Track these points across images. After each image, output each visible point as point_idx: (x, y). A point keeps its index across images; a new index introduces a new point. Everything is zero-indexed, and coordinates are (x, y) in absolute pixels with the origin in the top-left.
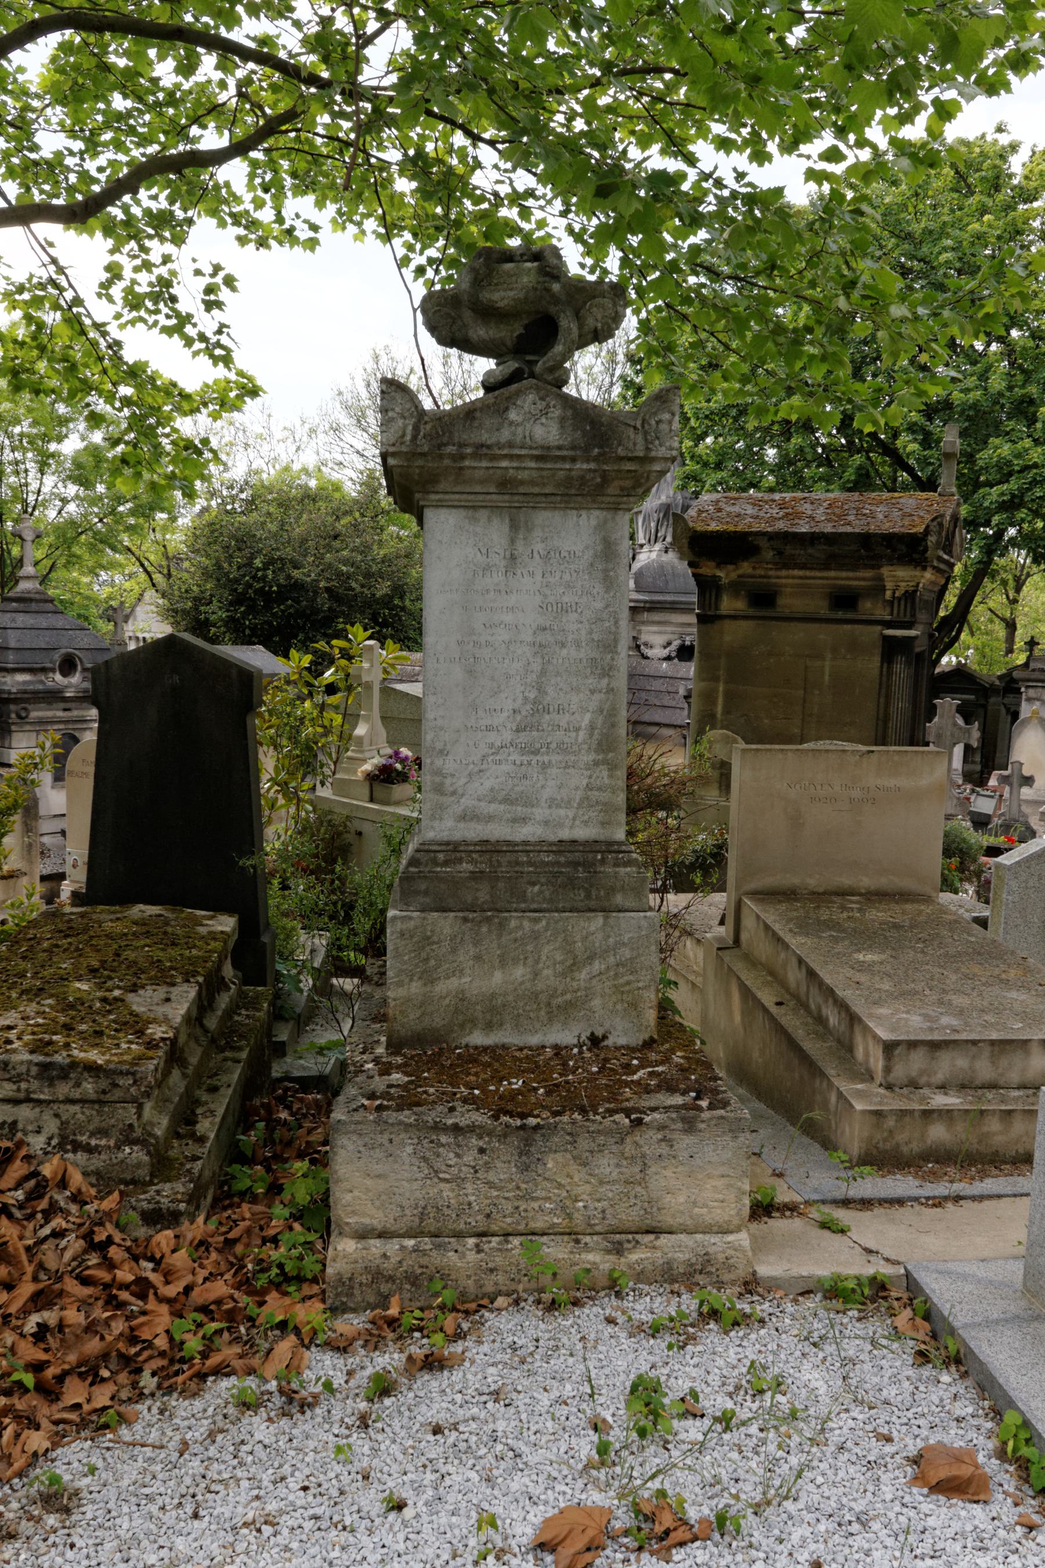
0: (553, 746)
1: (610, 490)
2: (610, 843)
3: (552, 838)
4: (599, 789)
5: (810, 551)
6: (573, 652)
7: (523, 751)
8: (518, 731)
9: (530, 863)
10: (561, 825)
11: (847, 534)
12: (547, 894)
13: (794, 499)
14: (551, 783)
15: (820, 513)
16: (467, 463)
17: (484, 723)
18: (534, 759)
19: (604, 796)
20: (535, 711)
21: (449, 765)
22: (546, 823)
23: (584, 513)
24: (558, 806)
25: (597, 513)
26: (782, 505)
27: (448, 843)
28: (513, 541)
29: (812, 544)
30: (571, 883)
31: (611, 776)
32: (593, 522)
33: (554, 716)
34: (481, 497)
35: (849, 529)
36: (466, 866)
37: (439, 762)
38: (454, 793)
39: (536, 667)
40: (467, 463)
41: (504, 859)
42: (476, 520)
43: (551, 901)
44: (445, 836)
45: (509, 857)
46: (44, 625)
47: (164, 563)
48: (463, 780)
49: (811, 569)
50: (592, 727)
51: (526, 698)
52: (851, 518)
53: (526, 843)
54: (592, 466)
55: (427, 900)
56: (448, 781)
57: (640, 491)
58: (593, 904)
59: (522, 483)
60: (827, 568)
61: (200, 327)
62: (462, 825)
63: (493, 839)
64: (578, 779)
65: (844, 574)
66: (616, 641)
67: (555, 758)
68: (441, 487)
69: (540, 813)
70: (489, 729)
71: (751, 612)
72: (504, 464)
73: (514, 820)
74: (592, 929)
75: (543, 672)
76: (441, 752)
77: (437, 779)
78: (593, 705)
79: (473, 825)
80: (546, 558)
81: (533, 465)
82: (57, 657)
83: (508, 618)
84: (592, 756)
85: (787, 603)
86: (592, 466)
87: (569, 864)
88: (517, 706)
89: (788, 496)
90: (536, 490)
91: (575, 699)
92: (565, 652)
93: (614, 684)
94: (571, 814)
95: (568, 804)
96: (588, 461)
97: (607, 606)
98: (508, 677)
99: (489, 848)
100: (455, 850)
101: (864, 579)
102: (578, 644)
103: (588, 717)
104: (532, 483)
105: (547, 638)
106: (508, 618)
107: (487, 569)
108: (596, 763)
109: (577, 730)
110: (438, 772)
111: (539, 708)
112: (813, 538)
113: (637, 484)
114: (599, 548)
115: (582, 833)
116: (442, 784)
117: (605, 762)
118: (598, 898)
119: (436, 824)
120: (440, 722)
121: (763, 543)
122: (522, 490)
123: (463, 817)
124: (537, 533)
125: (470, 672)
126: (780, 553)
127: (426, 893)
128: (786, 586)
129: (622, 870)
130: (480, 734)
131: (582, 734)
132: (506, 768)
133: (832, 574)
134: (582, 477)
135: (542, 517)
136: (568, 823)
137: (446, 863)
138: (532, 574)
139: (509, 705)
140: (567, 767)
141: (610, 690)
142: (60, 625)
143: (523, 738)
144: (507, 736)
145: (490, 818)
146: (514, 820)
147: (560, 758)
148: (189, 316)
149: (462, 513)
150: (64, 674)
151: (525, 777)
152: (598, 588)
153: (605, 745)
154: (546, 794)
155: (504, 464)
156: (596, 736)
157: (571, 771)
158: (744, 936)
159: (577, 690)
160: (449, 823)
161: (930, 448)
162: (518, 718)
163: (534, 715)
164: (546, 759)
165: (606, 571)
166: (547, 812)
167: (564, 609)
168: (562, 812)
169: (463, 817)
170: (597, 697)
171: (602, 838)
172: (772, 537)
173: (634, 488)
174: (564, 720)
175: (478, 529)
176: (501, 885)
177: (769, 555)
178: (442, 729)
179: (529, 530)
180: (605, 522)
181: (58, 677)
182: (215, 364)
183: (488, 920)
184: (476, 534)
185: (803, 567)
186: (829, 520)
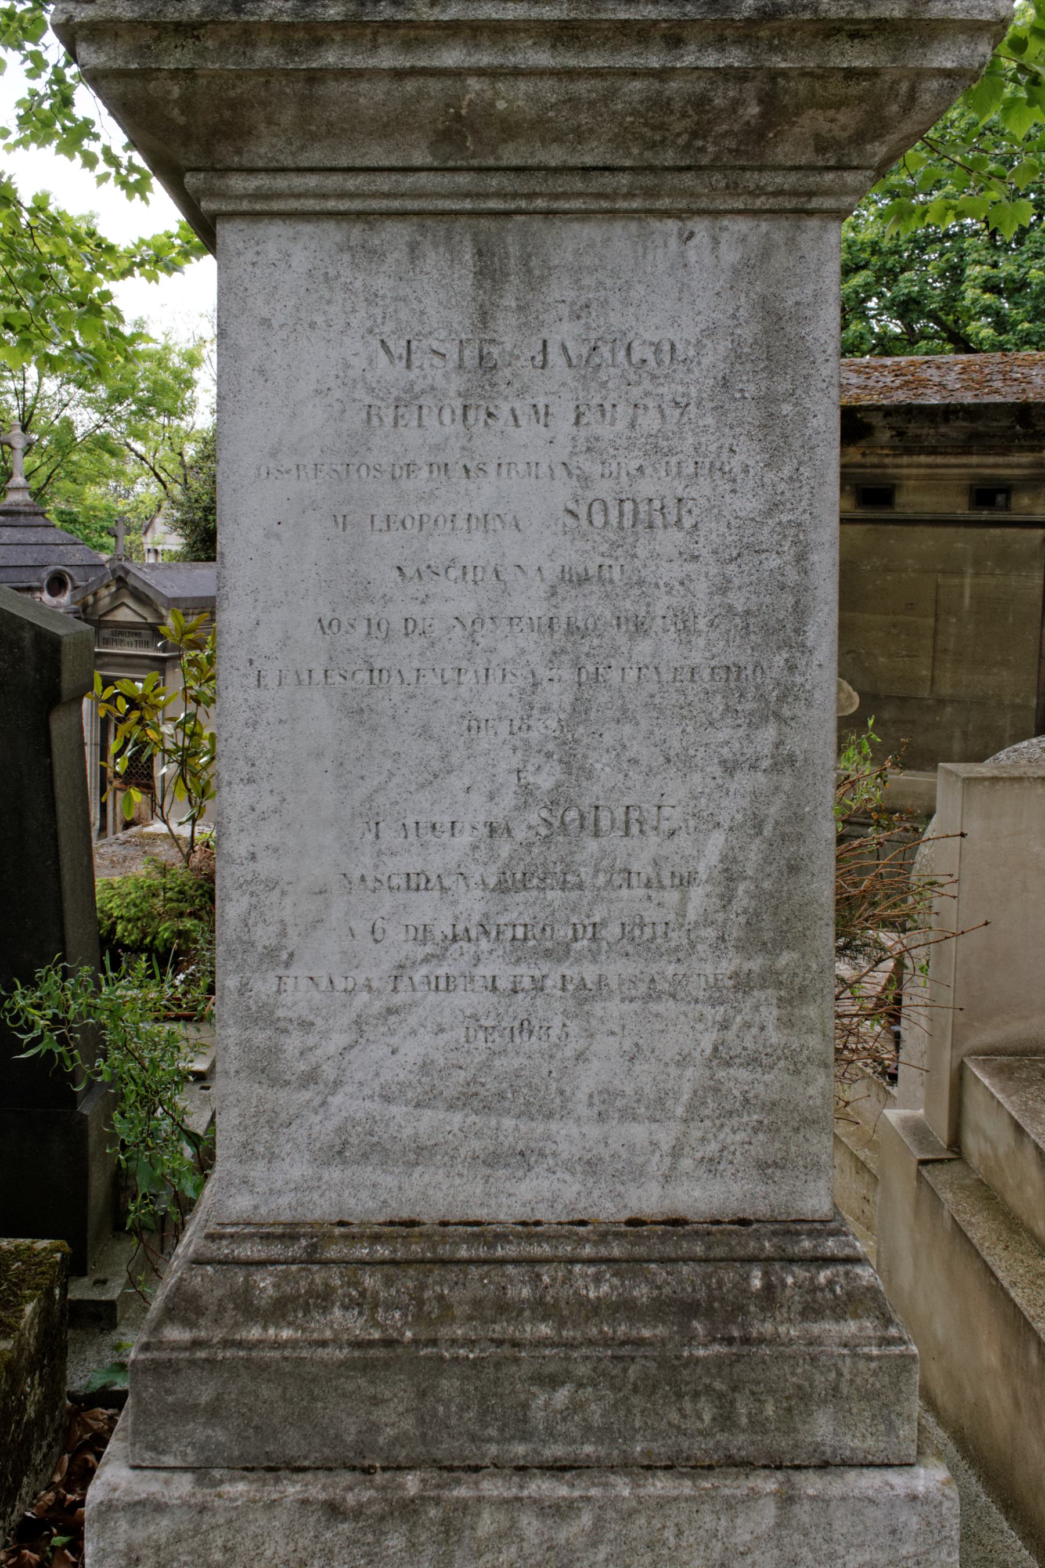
0: (613, 931)
1: (784, 152)
2: (790, 1227)
3: (608, 1208)
4: (753, 1061)
5: (942, 430)
6: (672, 652)
7: (519, 948)
8: (502, 888)
9: (542, 1309)
10: (638, 1174)
11: (997, 405)
12: (596, 1412)
13: (912, 364)
14: (604, 1044)
15: (952, 380)
16: (330, 57)
17: (399, 865)
18: (553, 973)
19: (768, 1084)
20: (556, 829)
21: (297, 997)
22: (592, 1166)
23: (701, 227)
24: (628, 1115)
25: (742, 225)
26: (898, 372)
27: (289, 1234)
28: (484, 317)
29: (946, 420)
30: (672, 1377)
31: (786, 1023)
32: (730, 255)
33: (615, 842)
34: (384, 183)
35: (998, 399)
36: (340, 1318)
37: (264, 986)
38: (310, 1078)
39: (558, 694)
40: (330, 57)
41: (462, 1291)
42: (375, 255)
43: (604, 1434)
44: (282, 1207)
45: (478, 1284)
46: (33, 540)
47: (181, 472)
48: (339, 1040)
49: (946, 454)
50: (729, 874)
51: (527, 791)
52: (998, 384)
53: (529, 1229)
54: (735, 57)
55: (220, 1435)
56: (292, 1043)
57: (879, 150)
58: (740, 1443)
59: (509, 129)
60: (967, 451)
61: (104, 140)
62: (334, 1174)
63: (429, 1214)
64: (687, 1032)
65: (991, 460)
66: (800, 612)
67: (616, 969)
68: (260, 151)
69: (569, 1136)
70: (416, 883)
71: (860, 513)
72: (451, 57)
73: (493, 1160)
74: (742, 1537)
75: (580, 709)
76: (271, 954)
77: (261, 1037)
78: (732, 808)
79: (368, 1173)
80: (587, 365)
81: (543, 58)
82: (45, 575)
83: (473, 548)
84: (730, 964)
85: (908, 501)
86: (735, 57)
87: (659, 1309)
88: (499, 812)
89: (903, 360)
90: (555, 155)
91: (676, 790)
92: (644, 647)
93: (796, 743)
94: (666, 1136)
95: (658, 1107)
96: (720, 43)
97: (774, 507)
98: (474, 726)
99: (419, 1250)
100: (312, 1258)
101: (1019, 466)
102: (684, 624)
103: (717, 841)
104: (541, 127)
105: (593, 604)
106: (473, 548)
107: (408, 400)
108: (743, 983)
109: (685, 882)
110: (263, 1016)
111: (569, 817)
112: (948, 412)
113: (874, 127)
114: (748, 333)
115: (698, 1196)
116: (275, 1051)
117: (770, 978)
118: (757, 1424)
119: (258, 1170)
120: (266, 866)
121: (877, 420)
122: (510, 155)
123: (338, 1152)
124: (560, 289)
125: (358, 713)
126: (901, 434)
127: (214, 1412)
128: (908, 477)
129: (828, 1328)
130: (388, 901)
131: (697, 894)
132: (468, 1000)
133: (974, 460)
134: (701, 102)
135: (572, 241)
136: (657, 1164)
137: (280, 1310)
138: (543, 415)
139: (477, 811)
140: (652, 996)
141: (784, 762)
142: (50, 539)
143: (520, 909)
144: (473, 904)
145: (421, 1153)
146: (493, 1160)
147: (626, 968)
148: (88, 123)
149: (332, 233)
150: (53, 593)
151: (525, 1027)
152: (747, 454)
153: (769, 927)
154: (587, 1080)
155: (451, 57)
156: (742, 899)
157: (666, 1007)
158: (972, 1143)
159: (687, 763)
160: (298, 1169)
161: (1006, 332)
162: (505, 848)
163: (554, 838)
164: (590, 973)
165: (767, 400)
166: (594, 1131)
167: (644, 519)
168: (639, 1132)
169: (338, 1152)
170: (743, 781)
171: (762, 1209)
172: (888, 412)
173: (860, 138)
174: (642, 853)
175: (382, 284)
176: (448, 1385)
177: (885, 436)
178: (271, 885)
179: (534, 282)
180: (766, 254)
181: (46, 597)
182: (130, 197)
183: (408, 1510)
184: (372, 298)
185: (933, 451)
186: (966, 388)
